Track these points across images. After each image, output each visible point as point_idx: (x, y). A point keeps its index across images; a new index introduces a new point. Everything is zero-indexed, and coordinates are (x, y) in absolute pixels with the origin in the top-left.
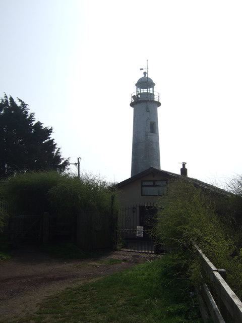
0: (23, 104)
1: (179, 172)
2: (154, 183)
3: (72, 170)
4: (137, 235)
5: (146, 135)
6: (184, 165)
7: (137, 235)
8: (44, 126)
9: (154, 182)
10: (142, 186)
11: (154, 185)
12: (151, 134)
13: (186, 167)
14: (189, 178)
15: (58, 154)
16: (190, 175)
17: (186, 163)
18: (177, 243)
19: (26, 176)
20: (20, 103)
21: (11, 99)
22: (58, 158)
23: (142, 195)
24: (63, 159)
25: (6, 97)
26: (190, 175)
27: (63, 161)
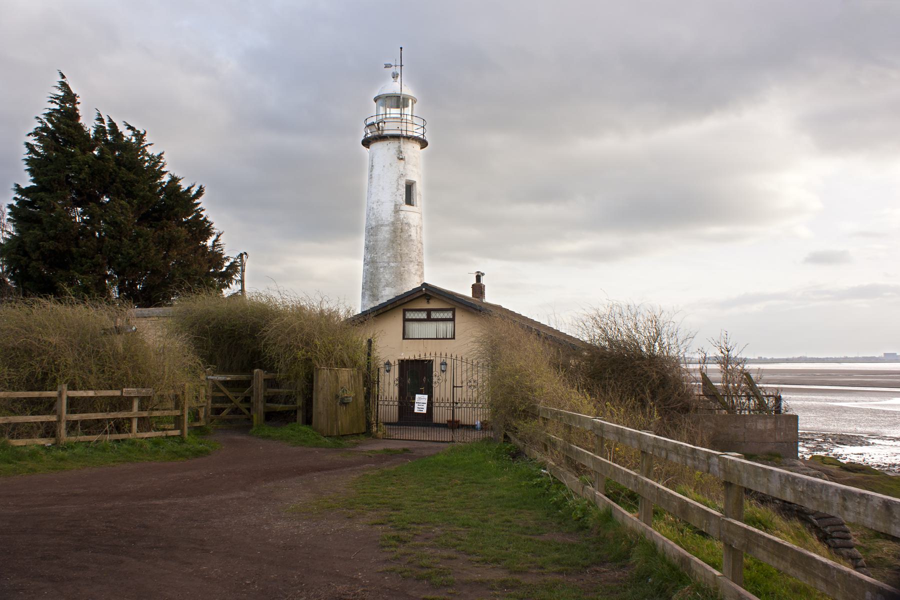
0: (140, 136)
1: (469, 293)
2: (429, 315)
3: (342, 313)
4: (416, 411)
5: (397, 210)
6: (478, 278)
7: (416, 411)
8: (184, 185)
9: (429, 311)
10: (405, 320)
11: (429, 319)
12: (408, 207)
13: (484, 281)
14: (487, 304)
15: (217, 249)
16: (490, 298)
17: (483, 274)
18: (285, 403)
19: (199, 303)
20: (130, 132)
21: (113, 125)
22: (216, 258)
23: (404, 338)
24: (227, 259)
25: (101, 120)
26: (490, 298)
27: (227, 264)
